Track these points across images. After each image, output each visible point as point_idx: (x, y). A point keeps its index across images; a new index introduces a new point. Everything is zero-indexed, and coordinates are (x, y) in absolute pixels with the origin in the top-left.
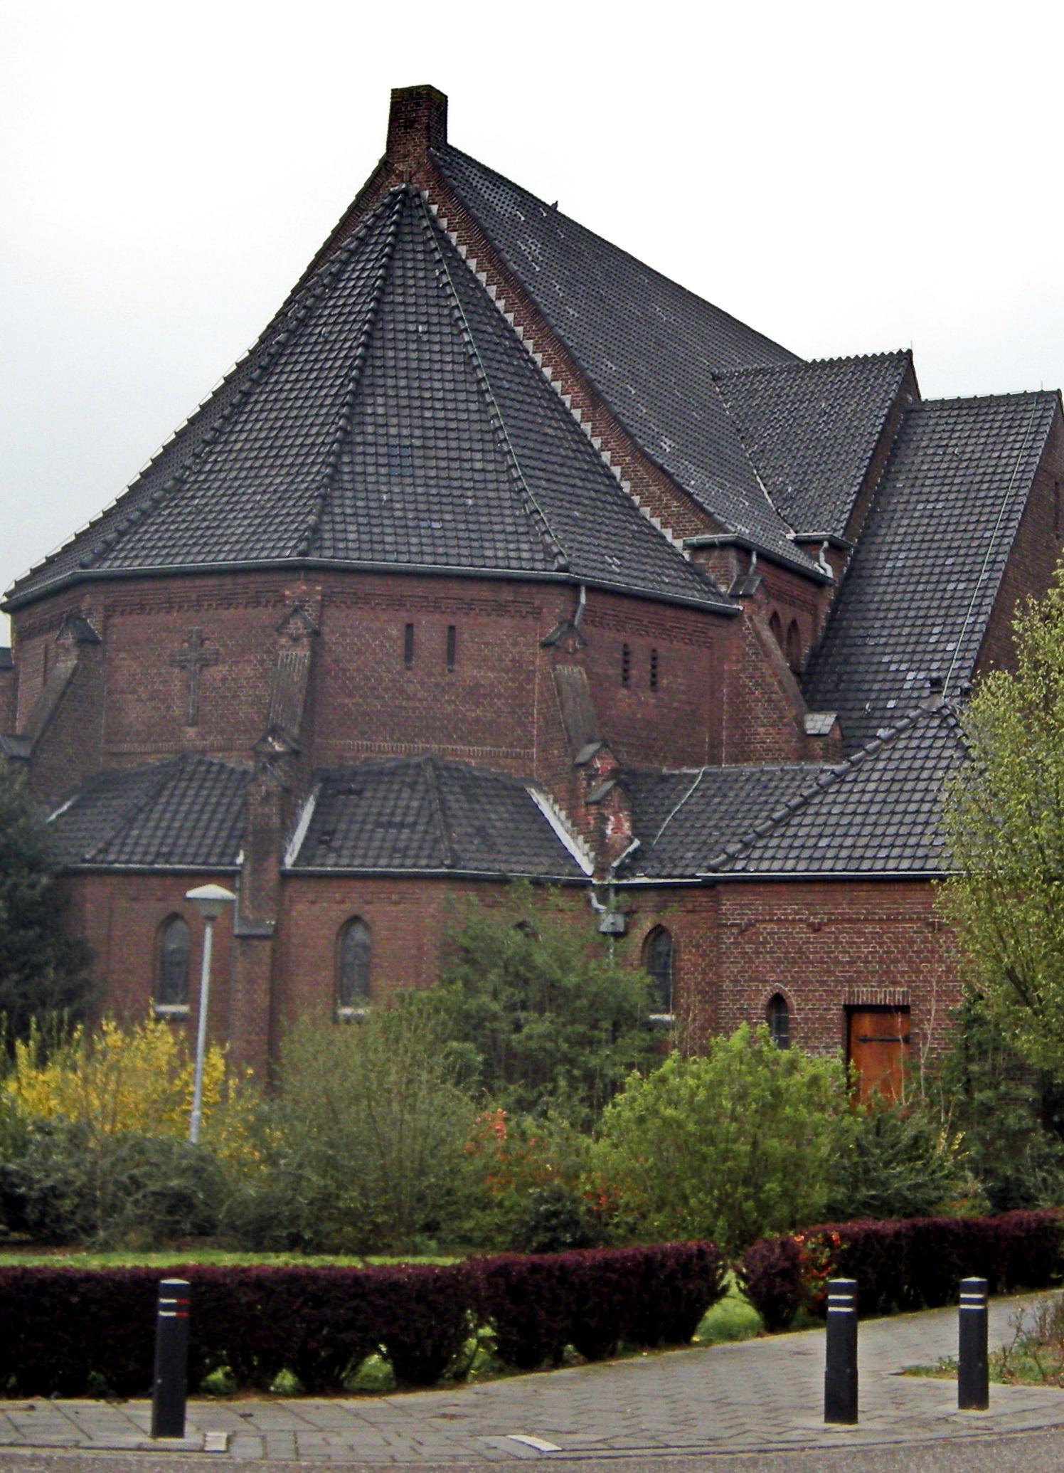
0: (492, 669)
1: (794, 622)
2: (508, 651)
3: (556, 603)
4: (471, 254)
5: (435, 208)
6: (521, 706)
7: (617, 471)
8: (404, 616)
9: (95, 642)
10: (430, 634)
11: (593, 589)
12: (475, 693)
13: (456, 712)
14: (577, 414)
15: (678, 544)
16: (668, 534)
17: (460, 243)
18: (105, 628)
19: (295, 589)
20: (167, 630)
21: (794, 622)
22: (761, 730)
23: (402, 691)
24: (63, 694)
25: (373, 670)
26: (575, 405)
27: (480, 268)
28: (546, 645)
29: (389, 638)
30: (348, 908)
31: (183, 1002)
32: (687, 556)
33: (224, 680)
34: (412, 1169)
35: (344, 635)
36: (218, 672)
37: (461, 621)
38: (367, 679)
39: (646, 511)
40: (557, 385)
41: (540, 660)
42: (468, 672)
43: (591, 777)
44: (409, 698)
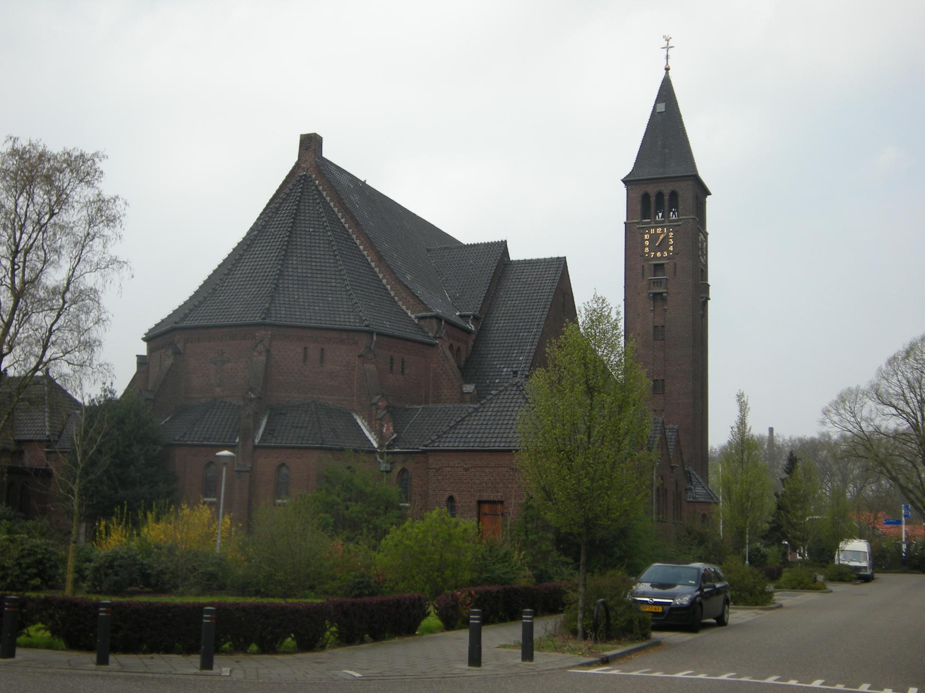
4: (331, 200)
7: (389, 287)
11: (379, 334)
15: (413, 316)
28: (360, 356)
39: (400, 303)
40: (365, 253)
43: (378, 409)
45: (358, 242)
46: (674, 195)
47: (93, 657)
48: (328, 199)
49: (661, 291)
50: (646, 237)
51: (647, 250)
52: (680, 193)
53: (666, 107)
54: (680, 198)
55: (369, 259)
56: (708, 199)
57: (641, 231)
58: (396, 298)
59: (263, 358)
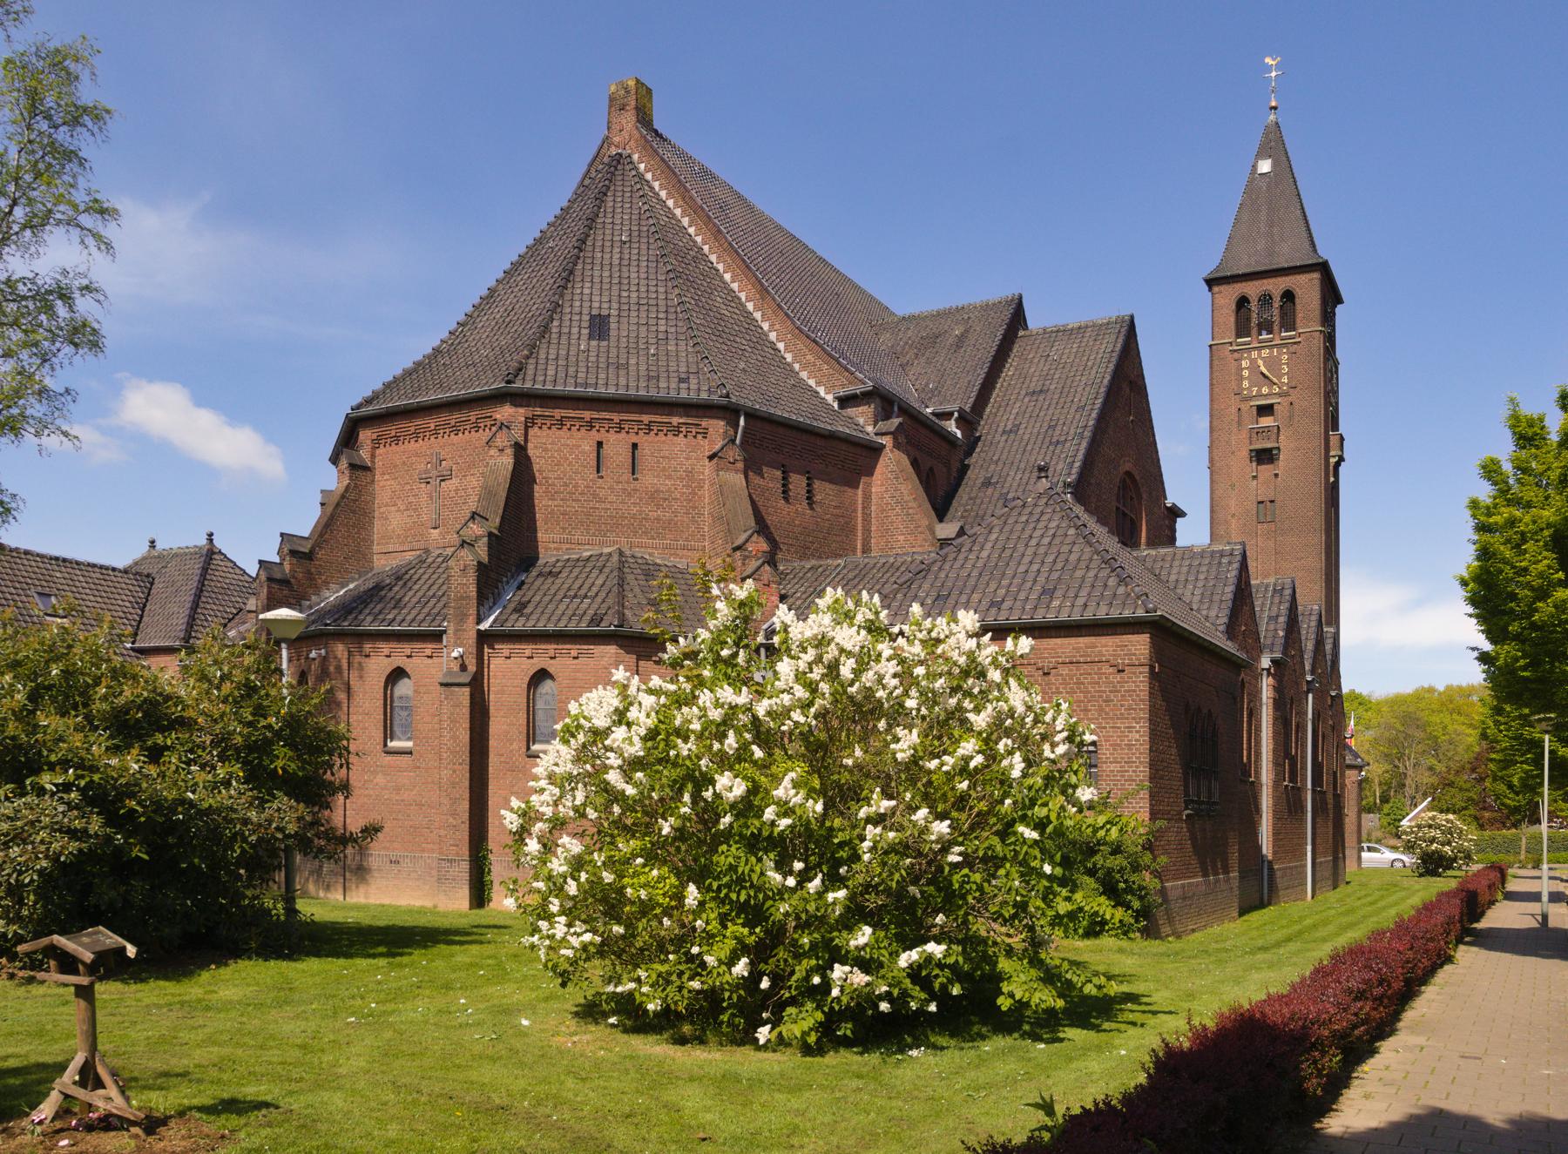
0: (669, 477)
1: (931, 469)
2: (681, 464)
3: (717, 427)
4: (655, 178)
5: (642, 166)
6: (694, 508)
7: (781, 346)
8: (595, 436)
9: (366, 469)
10: (617, 445)
11: (752, 416)
12: (654, 497)
13: (641, 512)
14: (750, 306)
15: (829, 398)
16: (822, 391)
17: (748, 300)
18: (373, 456)
19: (505, 412)
20: (417, 455)
21: (931, 469)
22: (901, 538)
23: (595, 495)
24: (338, 505)
25: (571, 478)
26: (748, 300)
27: (676, 205)
28: (711, 458)
29: (583, 452)
30: (538, 663)
31: (409, 739)
32: (836, 405)
33: (457, 490)
34: (1095, 864)
35: (546, 450)
36: (453, 484)
37: (641, 439)
38: (566, 485)
39: (804, 375)
40: (735, 286)
41: (707, 468)
42: (648, 479)
43: (745, 558)
44: (601, 501)
45: (720, 267)
46: (1289, 296)
47: (1551, 924)
48: (663, 194)
49: (1269, 445)
50: (1244, 364)
51: (1246, 384)
52: (1298, 292)
53: (1274, 165)
54: (1297, 301)
55: (743, 296)
56: (1339, 309)
57: (1236, 355)
58: (797, 366)
59: (507, 461)
